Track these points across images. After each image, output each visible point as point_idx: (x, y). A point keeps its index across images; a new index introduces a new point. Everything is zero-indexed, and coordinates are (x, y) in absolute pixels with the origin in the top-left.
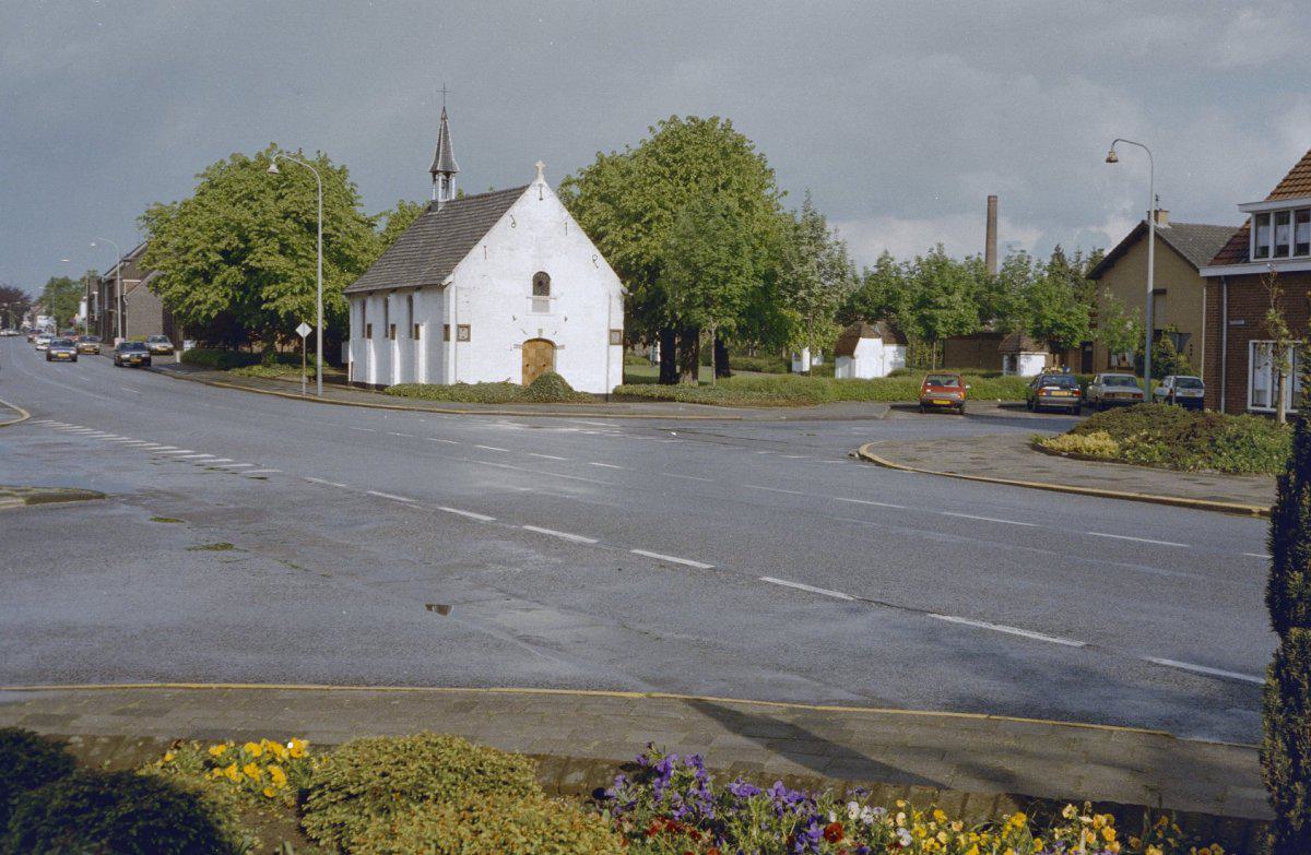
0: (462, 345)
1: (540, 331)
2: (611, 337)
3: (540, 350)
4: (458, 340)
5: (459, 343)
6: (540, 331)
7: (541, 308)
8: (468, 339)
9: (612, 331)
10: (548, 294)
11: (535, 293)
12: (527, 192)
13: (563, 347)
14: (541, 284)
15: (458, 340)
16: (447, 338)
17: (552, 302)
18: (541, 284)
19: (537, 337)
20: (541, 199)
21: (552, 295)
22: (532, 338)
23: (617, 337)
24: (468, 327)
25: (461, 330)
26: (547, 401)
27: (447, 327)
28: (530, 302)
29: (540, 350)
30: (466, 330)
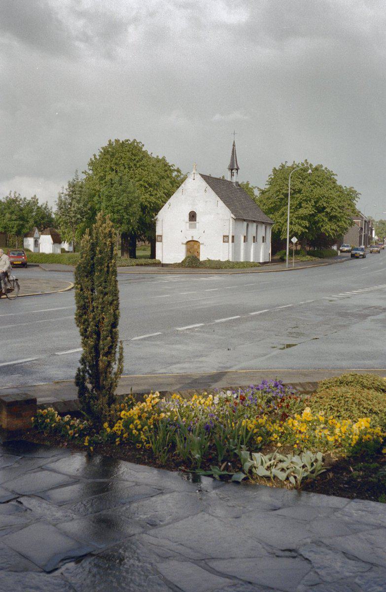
0: (226, 234)
1: (192, 237)
2: (224, 239)
3: (192, 246)
4: (228, 236)
5: (227, 235)
6: (192, 237)
7: (193, 227)
8: (224, 236)
9: (161, 241)
10: (195, 221)
11: (190, 221)
12: (187, 181)
13: (203, 244)
14: (193, 216)
15: (228, 236)
16: (233, 237)
17: (197, 224)
18: (193, 216)
19: (191, 239)
20: (194, 179)
21: (197, 221)
22: (189, 240)
23: (159, 239)
24: (224, 242)
25: (225, 238)
26: (193, 267)
27: (233, 241)
28: (188, 224)
29: (192, 246)
30: (160, 238)
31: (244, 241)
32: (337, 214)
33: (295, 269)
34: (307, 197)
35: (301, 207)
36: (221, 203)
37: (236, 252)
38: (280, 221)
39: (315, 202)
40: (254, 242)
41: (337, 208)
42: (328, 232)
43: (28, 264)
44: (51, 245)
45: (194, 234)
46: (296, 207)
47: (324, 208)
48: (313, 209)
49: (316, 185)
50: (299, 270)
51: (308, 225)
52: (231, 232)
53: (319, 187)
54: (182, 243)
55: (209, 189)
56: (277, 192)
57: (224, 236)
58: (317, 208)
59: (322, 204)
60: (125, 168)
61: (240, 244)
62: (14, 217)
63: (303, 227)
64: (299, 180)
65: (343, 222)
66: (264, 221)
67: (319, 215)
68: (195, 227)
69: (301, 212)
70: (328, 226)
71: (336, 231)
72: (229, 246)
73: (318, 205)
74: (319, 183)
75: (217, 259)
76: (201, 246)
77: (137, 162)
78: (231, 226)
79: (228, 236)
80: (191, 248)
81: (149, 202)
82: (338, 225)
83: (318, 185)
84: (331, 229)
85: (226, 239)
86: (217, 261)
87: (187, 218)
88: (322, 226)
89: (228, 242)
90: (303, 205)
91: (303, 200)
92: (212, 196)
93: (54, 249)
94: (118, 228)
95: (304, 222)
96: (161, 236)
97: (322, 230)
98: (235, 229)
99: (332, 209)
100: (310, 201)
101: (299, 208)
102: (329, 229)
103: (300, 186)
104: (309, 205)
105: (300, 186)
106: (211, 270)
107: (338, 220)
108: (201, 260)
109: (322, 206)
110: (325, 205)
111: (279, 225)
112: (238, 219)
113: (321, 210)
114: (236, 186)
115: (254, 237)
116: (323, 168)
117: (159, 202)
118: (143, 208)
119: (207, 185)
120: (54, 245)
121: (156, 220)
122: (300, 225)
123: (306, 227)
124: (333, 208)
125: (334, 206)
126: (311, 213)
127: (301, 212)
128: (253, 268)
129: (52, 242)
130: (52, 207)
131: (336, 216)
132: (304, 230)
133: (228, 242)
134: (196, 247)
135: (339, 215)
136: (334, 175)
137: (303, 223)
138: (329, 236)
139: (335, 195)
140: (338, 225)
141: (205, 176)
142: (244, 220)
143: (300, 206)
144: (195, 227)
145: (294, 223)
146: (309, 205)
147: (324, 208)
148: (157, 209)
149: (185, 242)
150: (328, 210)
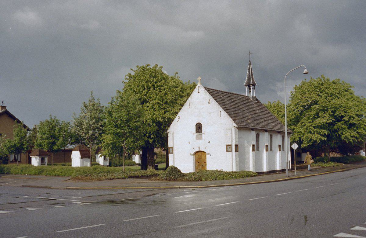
0: (280, 144)
1: (199, 148)
5: (230, 144)
6: (199, 148)
8: (227, 146)
9: (172, 153)
14: (199, 128)
16: (236, 146)
18: (199, 128)
20: (199, 93)
21: (203, 132)
24: (227, 151)
25: (228, 147)
27: (236, 150)
28: (195, 135)
31: (236, 151)
32: (355, 122)
33: (215, 186)
34: (323, 107)
35: (319, 117)
36: (224, 113)
37: (242, 160)
38: (301, 131)
39: (332, 112)
40: (280, 150)
41: (354, 116)
42: (348, 138)
43: (289, 168)
44: (80, 160)
45: (201, 145)
46: (314, 117)
47: (342, 117)
48: (330, 118)
49: (334, 97)
50: (316, 176)
51: (327, 134)
52: (234, 141)
53: (337, 98)
54: (191, 154)
55: (213, 101)
56: (296, 105)
57: (227, 146)
58: (335, 117)
59: (340, 114)
60: (144, 90)
61: (249, 153)
62: (45, 136)
63: (321, 135)
64: (316, 93)
65: (362, 129)
66: (280, 131)
67: (339, 124)
68: (201, 138)
69: (319, 121)
70: (348, 134)
71: (356, 138)
72: (232, 155)
73: (335, 115)
74: (337, 94)
75: (215, 169)
76: (207, 156)
77: (156, 83)
78: (234, 136)
79: (230, 146)
80: (199, 159)
81: (163, 118)
82: (357, 132)
83: (336, 96)
84: (351, 136)
85: (229, 148)
86: (215, 171)
87: (194, 129)
88: (342, 133)
89: (231, 151)
90: (320, 115)
91: (320, 110)
92: (215, 107)
93: (82, 163)
94: (124, 141)
95: (323, 130)
96: (172, 148)
97: (343, 137)
98: (239, 138)
99: (350, 118)
100: (327, 110)
101: (317, 118)
102: (349, 136)
103: (318, 98)
104: (327, 114)
105: (318, 98)
106: (190, 183)
107: (357, 128)
108: (208, 169)
109: (340, 115)
110: (343, 114)
111: (300, 135)
112: (240, 128)
113: (339, 119)
114: (253, 100)
115: (280, 146)
116: (341, 82)
117: (172, 117)
118: (159, 124)
119: (211, 97)
120: (82, 160)
121: (168, 133)
122: (319, 134)
123: (324, 135)
124: (351, 116)
125: (352, 115)
126: (328, 121)
127: (319, 121)
128: (246, 179)
129: (80, 156)
130: (40, 122)
131: (354, 123)
132: (323, 138)
133: (231, 151)
134: (203, 157)
135: (357, 123)
136: (350, 87)
137: (322, 132)
138: (350, 142)
139: (351, 104)
140: (357, 132)
141: (218, 91)
142: (252, 129)
143: (317, 116)
144: (201, 138)
145: (312, 132)
146: (327, 114)
147: (342, 117)
148: (169, 122)
149: (193, 153)
150: (346, 118)
